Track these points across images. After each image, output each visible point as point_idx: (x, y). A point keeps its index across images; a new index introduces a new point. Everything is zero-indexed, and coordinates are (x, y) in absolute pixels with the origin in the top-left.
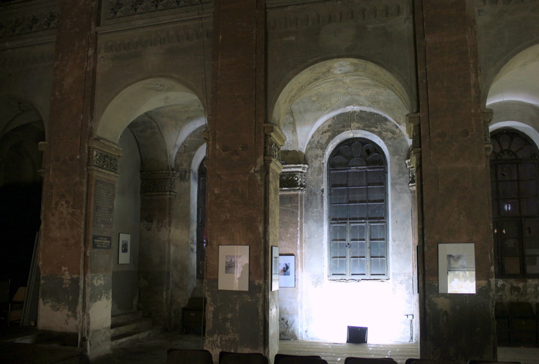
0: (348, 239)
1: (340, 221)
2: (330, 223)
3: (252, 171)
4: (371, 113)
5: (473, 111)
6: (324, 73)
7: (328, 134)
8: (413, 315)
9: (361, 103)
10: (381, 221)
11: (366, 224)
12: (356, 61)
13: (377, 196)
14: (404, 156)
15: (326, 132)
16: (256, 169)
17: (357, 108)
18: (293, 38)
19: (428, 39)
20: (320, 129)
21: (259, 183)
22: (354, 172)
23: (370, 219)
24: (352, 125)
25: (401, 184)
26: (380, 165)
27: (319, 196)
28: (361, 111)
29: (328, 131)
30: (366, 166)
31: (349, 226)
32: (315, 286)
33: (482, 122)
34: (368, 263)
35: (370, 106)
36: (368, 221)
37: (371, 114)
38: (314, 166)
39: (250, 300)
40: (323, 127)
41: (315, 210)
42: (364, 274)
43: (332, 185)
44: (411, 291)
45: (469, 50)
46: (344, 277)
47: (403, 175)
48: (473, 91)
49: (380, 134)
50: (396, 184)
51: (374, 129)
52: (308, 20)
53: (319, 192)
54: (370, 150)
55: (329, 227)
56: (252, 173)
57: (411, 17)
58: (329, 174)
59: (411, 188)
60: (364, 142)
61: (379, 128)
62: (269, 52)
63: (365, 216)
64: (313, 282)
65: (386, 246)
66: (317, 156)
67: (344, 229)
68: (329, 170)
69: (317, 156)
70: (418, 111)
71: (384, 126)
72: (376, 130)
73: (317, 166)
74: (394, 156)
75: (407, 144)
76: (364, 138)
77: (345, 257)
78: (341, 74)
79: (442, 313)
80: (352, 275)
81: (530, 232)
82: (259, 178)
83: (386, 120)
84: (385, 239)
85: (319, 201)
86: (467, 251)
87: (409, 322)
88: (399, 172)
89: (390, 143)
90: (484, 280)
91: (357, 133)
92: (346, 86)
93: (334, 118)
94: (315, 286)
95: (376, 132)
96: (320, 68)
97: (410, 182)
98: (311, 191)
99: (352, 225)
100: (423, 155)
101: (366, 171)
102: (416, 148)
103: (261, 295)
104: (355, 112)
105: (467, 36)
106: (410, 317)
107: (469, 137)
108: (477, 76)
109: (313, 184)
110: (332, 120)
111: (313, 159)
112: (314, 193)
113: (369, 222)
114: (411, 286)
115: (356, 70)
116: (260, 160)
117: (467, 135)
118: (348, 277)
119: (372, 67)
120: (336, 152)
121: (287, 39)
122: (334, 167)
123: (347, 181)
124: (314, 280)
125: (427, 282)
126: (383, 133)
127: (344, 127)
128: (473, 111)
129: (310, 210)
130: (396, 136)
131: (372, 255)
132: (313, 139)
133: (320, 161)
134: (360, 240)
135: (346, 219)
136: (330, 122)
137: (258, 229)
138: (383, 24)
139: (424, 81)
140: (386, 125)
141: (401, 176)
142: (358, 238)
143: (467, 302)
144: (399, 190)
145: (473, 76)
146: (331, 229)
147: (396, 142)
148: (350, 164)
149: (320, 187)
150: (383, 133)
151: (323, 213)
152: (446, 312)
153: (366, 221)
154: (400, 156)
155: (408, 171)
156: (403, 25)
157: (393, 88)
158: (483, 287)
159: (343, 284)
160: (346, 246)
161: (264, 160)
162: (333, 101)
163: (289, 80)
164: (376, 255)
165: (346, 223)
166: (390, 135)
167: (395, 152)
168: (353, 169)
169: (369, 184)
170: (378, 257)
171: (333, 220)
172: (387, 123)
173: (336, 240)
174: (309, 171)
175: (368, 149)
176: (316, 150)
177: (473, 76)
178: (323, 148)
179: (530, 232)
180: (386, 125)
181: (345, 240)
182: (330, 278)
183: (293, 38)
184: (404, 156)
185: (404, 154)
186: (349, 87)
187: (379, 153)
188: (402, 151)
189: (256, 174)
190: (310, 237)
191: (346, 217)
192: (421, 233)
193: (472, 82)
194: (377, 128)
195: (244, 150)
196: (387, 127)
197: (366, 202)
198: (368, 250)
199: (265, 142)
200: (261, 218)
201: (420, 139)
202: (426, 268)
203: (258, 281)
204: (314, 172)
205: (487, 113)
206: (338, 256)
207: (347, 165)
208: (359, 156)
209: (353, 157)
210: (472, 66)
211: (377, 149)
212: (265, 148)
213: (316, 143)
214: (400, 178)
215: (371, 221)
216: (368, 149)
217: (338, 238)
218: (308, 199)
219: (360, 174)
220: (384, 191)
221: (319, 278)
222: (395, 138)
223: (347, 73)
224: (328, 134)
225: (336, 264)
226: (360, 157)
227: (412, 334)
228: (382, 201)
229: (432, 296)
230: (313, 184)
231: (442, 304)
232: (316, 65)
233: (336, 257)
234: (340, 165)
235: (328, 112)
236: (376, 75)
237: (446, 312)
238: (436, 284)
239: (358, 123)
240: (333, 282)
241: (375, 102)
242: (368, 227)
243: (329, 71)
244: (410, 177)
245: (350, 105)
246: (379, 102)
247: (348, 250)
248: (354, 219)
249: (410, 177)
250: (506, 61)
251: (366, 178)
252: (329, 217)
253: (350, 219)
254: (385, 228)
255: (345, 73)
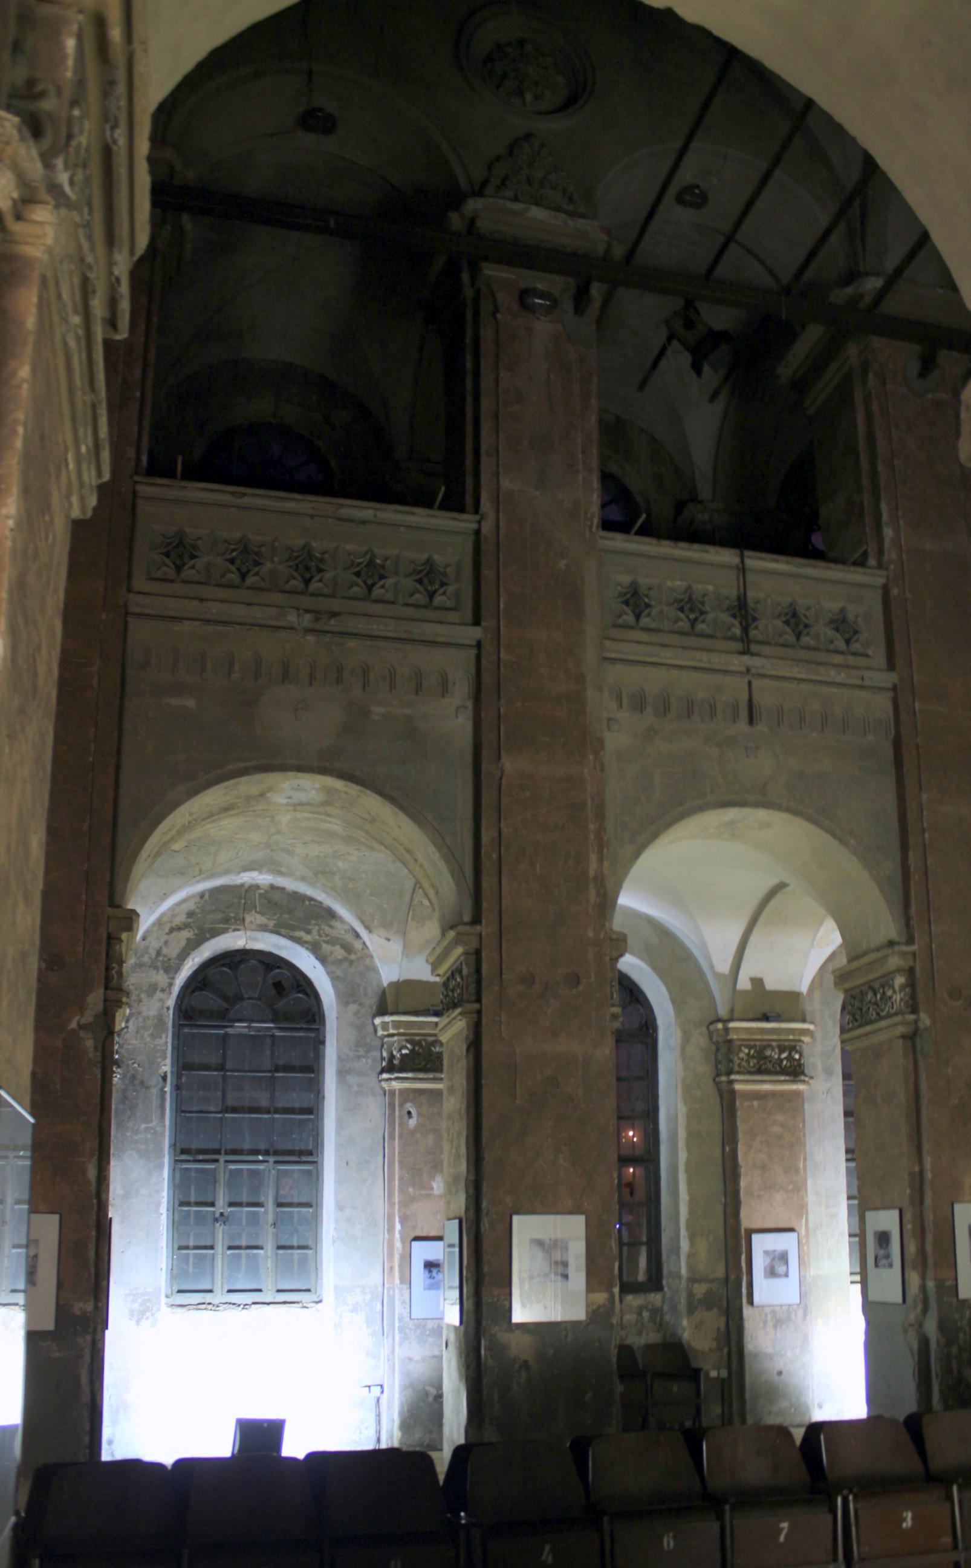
0: (221, 1206)
1: (201, 1157)
2: (176, 1161)
3: (74, 1025)
4: (296, 893)
5: (591, 934)
6: (248, 799)
7: (186, 934)
8: (382, 1386)
9: (283, 869)
10: (304, 1159)
11: (267, 1167)
12: (338, 784)
13: (296, 1099)
14: (371, 1006)
15: (179, 929)
16: (83, 1021)
17: (263, 879)
18: (190, 703)
19: (508, 764)
20: (165, 919)
21: (91, 1055)
22: (241, 1035)
23: (276, 1153)
24: (248, 918)
25: (360, 1074)
26: (308, 1022)
27: (155, 1091)
28: (273, 887)
29: (186, 926)
30: (272, 1021)
31: (223, 1169)
32: (138, 1322)
33: (608, 958)
34: (269, 1263)
35: (303, 879)
36: (271, 1159)
37: (297, 897)
38: (145, 1013)
39: (57, 1354)
40: (174, 916)
41: (143, 1126)
42: (260, 1290)
43: (183, 1066)
44: (378, 1328)
45: (589, 802)
46: (208, 1297)
47: (367, 1051)
48: (593, 893)
49: (315, 949)
50: (349, 1071)
51: (301, 934)
52: (231, 665)
53: (154, 1081)
54: (285, 984)
55: (173, 1171)
56: (73, 1030)
57: (470, 705)
58: (177, 1036)
59: (384, 1085)
60: (270, 962)
61: (315, 932)
62: (128, 726)
63: (263, 1146)
64: (132, 1312)
65: (315, 1221)
66: (153, 989)
67: (211, 1179)
68: (178, 1028)
69: (153, 989)
70: (476, 920)
71: (327, 929)
72: (308, 938)
73: (153, 1012)
74: (347, 1004)
75: (380, 979)
76: (270, 954)
77: (212, 1248)
78: (287, 804)
79: (517, 1366)
80: (229, 1291)
81: (632, 1194)
82: (89, 1043)
83: (331, 914)
84: (313, 1203)
85: (155, 1102)
86: (571, 1230)
87: (374, 1402)
88: (358, 1044)
89: (339, 973)
90: (600, 1291)
91: (256, 939)
92: (273, 830)
93: (202, 895)
94: (138, 1322)
95: (307, 942)
96: (248, 785)
97: (383, 1071)
98: (133, 1077)
99: (232, 1167)
100: (484, 1021)
101: (273, 1036)
102: (468, 1001)
103: (89, 1338)
104: (257, 887)
105: (586, 771)
106: (376, 1391)
107: (581, 988)
108: (601, 860)
109: (139, 1058)
110: (198, 899)
111: (143, 996)
112: (142, 1083)
113: (276, 1162)
114: (379, 1316)
115: (326, 803)
116: (95, 999)
117: (578, 983)
118: (218, 1297)
119: (373, 803)
120: (199, 981)
121: (174, 701)
122: (191, 1018)
123: (224, 1056)
124: (136, 1306)
125: (486, 1299)
126: (324, 946)
127: (226, 920)
128: (591, 934)
129: (131, 1124)
130: (353, 957)
131: (280, 1244)
132: (146, 943)
133: (161, 1000)
134: (249, 1205)
135: (217, 1152)
136: (191, 906)
137: (84, 1172)
138: (409, 711)
139: (494, 856)
140: (331, 927)
141: (361, 1052)
142: (244, 1199)
143: (569, 1340)
144: (356, 1088)
145: (593, 857)
146: (178, 1175)
147: (352, 970)
148: (231, 1015)
149: (159, 1066)
150: (324, 946)
151: (163, 1134)
152: (526, 1365)
153: (267, 1158)
154: (361, 1004)
155: (378, 1043)
156: (452, 720)
157: (408, 857)
158: (599, 1307)
159: (206, 1315)
160: (216, 1220)
161: (105, 1000)
162: (223, 857)
163: (176, 805)
164: (288, 1244)
165: (217, 1161)
166: (339, 953)
167: (348, 995)
168: (240, 1027)
169: (277, 1069)
170: (291, 1247)
171: (183, 1152)
172: (334, 923)
173: (188, 1204)
174: (130, 1024)
175: (280, 982)
176: (153, 973)
177: (593, 857)
178: (171, 969)
179: (632, 1194)
180: (331, 927)
181: (212, 1204)
182: (171, 1301)
183: (190, 703)
184: (371, 1006)
185: (372, 1001)
186: (279, 832)
187: (306, 994)
188: (366, 994)
189: (82, 1034)
190: (127, 1196)
191: (216, 1146)
192: (471, 1191)
193: (592, 873)
194: (308, 932)
195: (53, 970)
196: (334, 933)
197: (269, 1112)
198: (271, 1230)
199: (107, 955)
200: (91, 1144)
201: (479, 982)
202: (486, 1269)
203: (81, 1305)
204: (145, 1028)
205: (617, 940)
206: (191, 1243)
207: (223, 1016)
208: (256, 996)
209: (241, 998)
210: (592, 836)
211: (303, 983)
212: (108, 968)
213: (153, 953)
214: (359, 1057)
215: (280, 1158)
216: (280, 982)
217: (193, 1199)
218: (126, 1098)
219: (255, 1040)
220: (315, 1087)
221: (149, 1301)
222: (351, 963)
223: (302, 804)
224: (186, 934)
225: (187, 1263)
226: (259, 999)
227: (379, 1432)
228: (309, 1111)
229: (496, 1328)
230: (139, 1058)
231: (519, 1347)
232: (244, 779)
233: (187, 1248)
234: (210, 1014)
235: (198, 882)
236: (373, 821)
237: (526, 1362)
238: (507, 1303)
239: (261, 913)
240: (180, 1310)
241: (323, 873)
242: (273, 1172)
243: (262, 795)
244: (383, 1059)
245: (253, 869)
246: (334, 874)
247: (220, 1230)
248: (234, 1152)
249: (383, 1059)
250: (655, 836)
251: (272, 1053)
252: (173, 1146)
253: (226, 1153)
254: (314, 1178)
255: (295, 805)
